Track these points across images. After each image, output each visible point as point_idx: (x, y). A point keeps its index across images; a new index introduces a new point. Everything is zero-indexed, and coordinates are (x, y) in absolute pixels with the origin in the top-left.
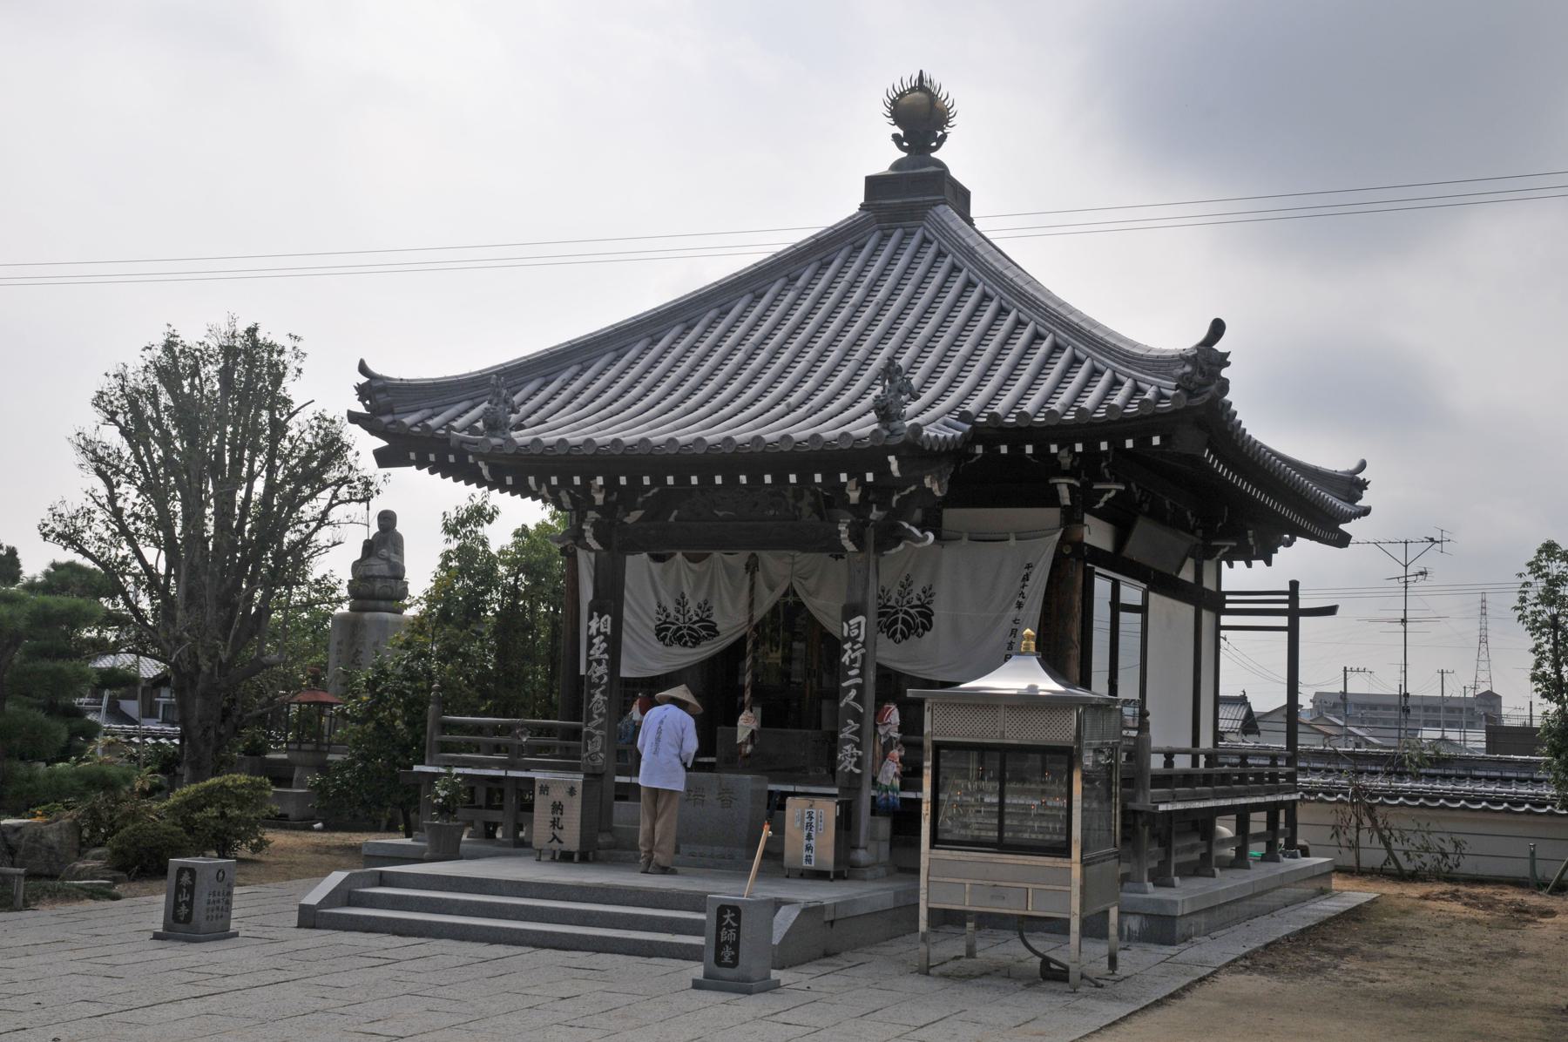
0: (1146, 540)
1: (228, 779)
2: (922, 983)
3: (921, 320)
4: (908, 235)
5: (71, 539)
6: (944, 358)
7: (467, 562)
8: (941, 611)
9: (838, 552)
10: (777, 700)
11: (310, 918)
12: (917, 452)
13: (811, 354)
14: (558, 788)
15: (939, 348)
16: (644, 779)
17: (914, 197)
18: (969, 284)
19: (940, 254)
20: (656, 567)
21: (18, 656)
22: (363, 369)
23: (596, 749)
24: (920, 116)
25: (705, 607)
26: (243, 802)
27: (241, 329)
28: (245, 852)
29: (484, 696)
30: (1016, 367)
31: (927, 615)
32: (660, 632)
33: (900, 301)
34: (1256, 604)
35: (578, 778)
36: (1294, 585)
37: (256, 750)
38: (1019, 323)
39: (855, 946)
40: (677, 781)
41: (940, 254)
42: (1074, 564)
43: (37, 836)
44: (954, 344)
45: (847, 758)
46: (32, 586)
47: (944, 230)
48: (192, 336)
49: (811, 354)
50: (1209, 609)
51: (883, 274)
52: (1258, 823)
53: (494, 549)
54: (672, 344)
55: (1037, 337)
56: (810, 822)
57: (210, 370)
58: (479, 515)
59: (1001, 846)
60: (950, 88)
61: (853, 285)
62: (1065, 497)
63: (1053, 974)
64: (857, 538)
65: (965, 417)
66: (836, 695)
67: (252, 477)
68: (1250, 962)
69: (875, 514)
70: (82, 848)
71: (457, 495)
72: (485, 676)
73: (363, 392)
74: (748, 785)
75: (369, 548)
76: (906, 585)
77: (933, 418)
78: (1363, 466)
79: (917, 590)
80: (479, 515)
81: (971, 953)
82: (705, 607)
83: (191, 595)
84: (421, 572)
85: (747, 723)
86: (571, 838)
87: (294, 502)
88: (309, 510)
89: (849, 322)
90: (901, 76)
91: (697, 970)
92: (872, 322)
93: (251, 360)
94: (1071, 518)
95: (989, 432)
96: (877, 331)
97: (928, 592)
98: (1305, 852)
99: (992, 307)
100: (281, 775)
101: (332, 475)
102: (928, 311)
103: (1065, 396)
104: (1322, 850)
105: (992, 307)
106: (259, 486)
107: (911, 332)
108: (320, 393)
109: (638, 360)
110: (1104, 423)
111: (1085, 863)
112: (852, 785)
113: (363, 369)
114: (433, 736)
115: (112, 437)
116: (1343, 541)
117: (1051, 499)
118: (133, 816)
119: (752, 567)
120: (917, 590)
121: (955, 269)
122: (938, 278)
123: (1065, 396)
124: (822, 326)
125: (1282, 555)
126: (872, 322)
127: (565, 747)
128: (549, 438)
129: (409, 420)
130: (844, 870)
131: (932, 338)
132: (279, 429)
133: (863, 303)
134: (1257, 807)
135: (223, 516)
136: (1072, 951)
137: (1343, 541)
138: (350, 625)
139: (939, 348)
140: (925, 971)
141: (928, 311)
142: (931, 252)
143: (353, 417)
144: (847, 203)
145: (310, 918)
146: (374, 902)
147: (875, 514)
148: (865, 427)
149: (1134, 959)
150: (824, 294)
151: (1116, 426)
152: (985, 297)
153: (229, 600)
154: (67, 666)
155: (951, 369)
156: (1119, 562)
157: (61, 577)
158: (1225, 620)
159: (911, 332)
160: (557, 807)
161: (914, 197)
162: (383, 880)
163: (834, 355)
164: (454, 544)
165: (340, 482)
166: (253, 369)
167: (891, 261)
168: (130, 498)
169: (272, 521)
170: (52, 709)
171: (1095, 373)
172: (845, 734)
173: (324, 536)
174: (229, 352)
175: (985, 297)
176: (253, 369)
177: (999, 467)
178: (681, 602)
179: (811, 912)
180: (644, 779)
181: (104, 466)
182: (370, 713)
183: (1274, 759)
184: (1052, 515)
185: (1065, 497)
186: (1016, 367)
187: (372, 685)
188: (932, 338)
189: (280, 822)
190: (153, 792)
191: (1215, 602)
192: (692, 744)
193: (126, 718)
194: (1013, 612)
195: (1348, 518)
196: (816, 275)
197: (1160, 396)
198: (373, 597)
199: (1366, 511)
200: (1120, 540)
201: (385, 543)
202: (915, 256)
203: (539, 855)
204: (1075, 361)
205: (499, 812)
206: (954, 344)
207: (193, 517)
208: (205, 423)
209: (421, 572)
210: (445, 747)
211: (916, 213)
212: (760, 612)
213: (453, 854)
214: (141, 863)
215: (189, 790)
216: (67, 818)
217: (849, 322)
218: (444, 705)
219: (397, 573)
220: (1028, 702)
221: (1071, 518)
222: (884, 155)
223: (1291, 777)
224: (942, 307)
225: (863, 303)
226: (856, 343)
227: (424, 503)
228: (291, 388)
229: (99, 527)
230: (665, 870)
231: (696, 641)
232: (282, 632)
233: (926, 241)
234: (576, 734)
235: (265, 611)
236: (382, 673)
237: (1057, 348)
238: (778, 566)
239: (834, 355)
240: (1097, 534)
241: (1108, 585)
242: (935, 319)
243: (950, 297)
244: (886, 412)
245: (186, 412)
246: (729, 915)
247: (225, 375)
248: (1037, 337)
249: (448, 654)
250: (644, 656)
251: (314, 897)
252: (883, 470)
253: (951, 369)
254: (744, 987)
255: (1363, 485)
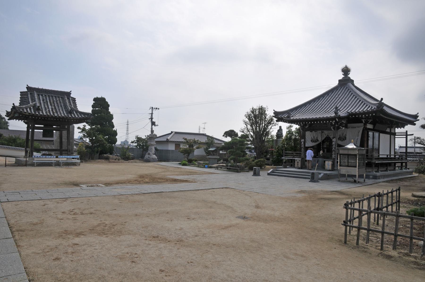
0: (378, 126)
1: (261, 159)
2: (338, 182)
3: (345, 99)
4: (344, 87)
5: (243, 132)
6: (347, 104)
7: (290, 132)
8: (347, 137)
9: (331, 130)
10: (325, 149)
11: (269, 174)
12: (340, 118)
13: (330, 105)
14: (298, 160)
15: (346, 103)
16: (307, 159)
17: (346, 82)
18: (352, 94)
19: (349, 90)
20: (311, 133)
21: (238, 145)
22: (274, 110)
23: (302, 155)
24: (346, 71)
25: (317, 137)
26: (263, 162)
27: (261, 106)
28: (263, 168)
29: (292, 149)
30: (356, 105)
31: (346, 138)
32: (311, 141)
33: (342, 97)
34: (401, 134)
35: (300, 159)
36: (407, 131)
37: (265, 156)
38: (358, 99)
39: (332, 179)
40: (311, 159)
41: (349, 90)
42: (365, 132)
43: (241, 166)
44: (349, 102)
45: (333, 156)
46: (239, 137)
47: (349, 86)
48: (255, 107)
49: (330, 105)
50: (392, 135)
51: (340, 93)
52: (404, 164)
53: (293, 131)
54: (312, 105)
55: (360, 101)
56: (328, 164)
57: (257, 111)
58: (291, 126)
59: (348, 166)
60: (349, 66)
61: (336, 95)
62: (364, 122)
63: (355, 182)
64: (334, 129)
65: (348, 113)
66: (332, 148)
67: (263, 123)
68: (387, 182)
69: (336, 125)
70: (246, 167)
71: (288, 125)
72: (292, 147)
73: (274, 113)
74: (321, 160)
75: (278, 131)
76: (343, 134)
77: (342, 113)
78: (418, 113)
79: (344, 135)
80: (291, 126)
81: (347, 179)
82: (317, 137)
83: (256, 138)
84: (284, 133)
85: (321, 152)
86: (300, 166)
87: (267, 126)
88: (269, 127)
89: (335, 100)
90: (343, 66)
91: (310, 180)
92: (338, 100)
93: (262, 110)
94: (365, 124)
95: (351, 114)
96: (339, 101)
97: (346, 135)
98: (408, 169)
99: (355, 97)
100: (268, 159)
101: (272, 123)
102: (346, 98)
103: (362, 109)
104: (411, 168)
105: (355, 97)
106: (263, 125)
107: (343, 101)
108: (270, 113)
109: (308, 107)
110: (367, 112)
111: (358, 169)
112: (334, 159)
113: (274, 110)
114: (284, 154)
115: (247, 120)
116: (415, 124)
117: (362, 122)
118: (251, 163)
119: (322, 132)
120: (344, 135)
121: (350, 92)
122: (348, 93)
123: (362, 109)
124: (332, 101)
125: (406, 127)
126: (338, 100)
127: (299, 155)
128: (295, 118)
129: (280, 116)
130: (333, 170)
131: (346, 102)
132: (265, 118)
133: (337, 97)
134: (404, 162)
135: (259, 128)
136: (357, 179)
137: (415, 124)
138: (276, 141)
139: (346, 103)
140: (339, 181)
141: (346, 98)
142: (347, 89)
143: (273, 116)
144: (336, 83)
145: (269, 174)
146: (276, 173)
147: (336, 125)
148: (333, 115)
149: (367, 180)
150: (332, 96)
151: (368, 113)
152: (354, 95)
153: (261, 138)
154: (243, 147)
155: (348, 106)
156: (373, 130)
157: (242, 136)
158: (396, 137)
159: (343, 101)
160: (298, 162)
161: (346, 82)
162: (277, 170)
163: (333, 105)
164: (288, 130)
165: (273, 123)
166: (262, 111)
167: (342, 91)
168: (249, 127)
169: (265, 129)
170: (241, 152)
171: (367, 105)
172: (333, 153)
173: (271, 130)
174: (259, 109)
175: (354, 95)
176: (262, 111)
177: (353, 119)
178: (314, 137)
179: (325, 174)
180: (307, 159)
181: (246, 123)
182: (278, 151)
183: (387, 155)
184: (362, 124)
185: (364, 122)
186: (356, 105)
187: (278, 148)
188: (346, 102)
189: (268, 165)
190: (253, 161)
191: (395, 134)
192: (313, 154)
193: (251, 152)
194: (357, 137)
195: (416, 121)
196: (332, 94)
197: (374, 108)
198: (279, 137)
199: (419, 120)
200: (374, 127)
201: (280, 130)
202: (345, 90)
203: (296, 168)
204: (365, 104)
205: (292, 163)
206: (349, 102)
207: (256, 129)
208: (257, 117)
209: (284, 133)
210: (285, 155)
211: (346, 84)
212: (323, 139)
213: (286, 168)
214: (251, 169)
215: (257, 160)
216: (244, 164)
217: (335, 100)
218: (286, 151)
219: (282, 134)
220: (352, 149)
221: (365, 124)
222: (341, 76)
223: (406, 158)
224: (348, 97)
225: (337, 97)
226: (336, 103)
227: (284, 126)
228: (266, 112)
229: (246, 131)
230: (310, 170)
231: (316, 142)
232: (267, 141)
233: (347, 88)
234: (300, 154)
235: (265, 139)
236: (279, 147)
237: (362, 102)
238: (326, 132)
239: (333, 105)
240: (369, 126)
241: (372, 133)
242: (347, 99)
243: (349, 96)
244: (336, 113)
245: (255, 116)
246: (313, 174)
247: (259, 112)
248: (360, 101)
249: (287, 144)
250: (309, 144)
251: (269, 172)
252: (336, 120)
253: (348, 106)
254: (315, 182)
255: (418, 116)
